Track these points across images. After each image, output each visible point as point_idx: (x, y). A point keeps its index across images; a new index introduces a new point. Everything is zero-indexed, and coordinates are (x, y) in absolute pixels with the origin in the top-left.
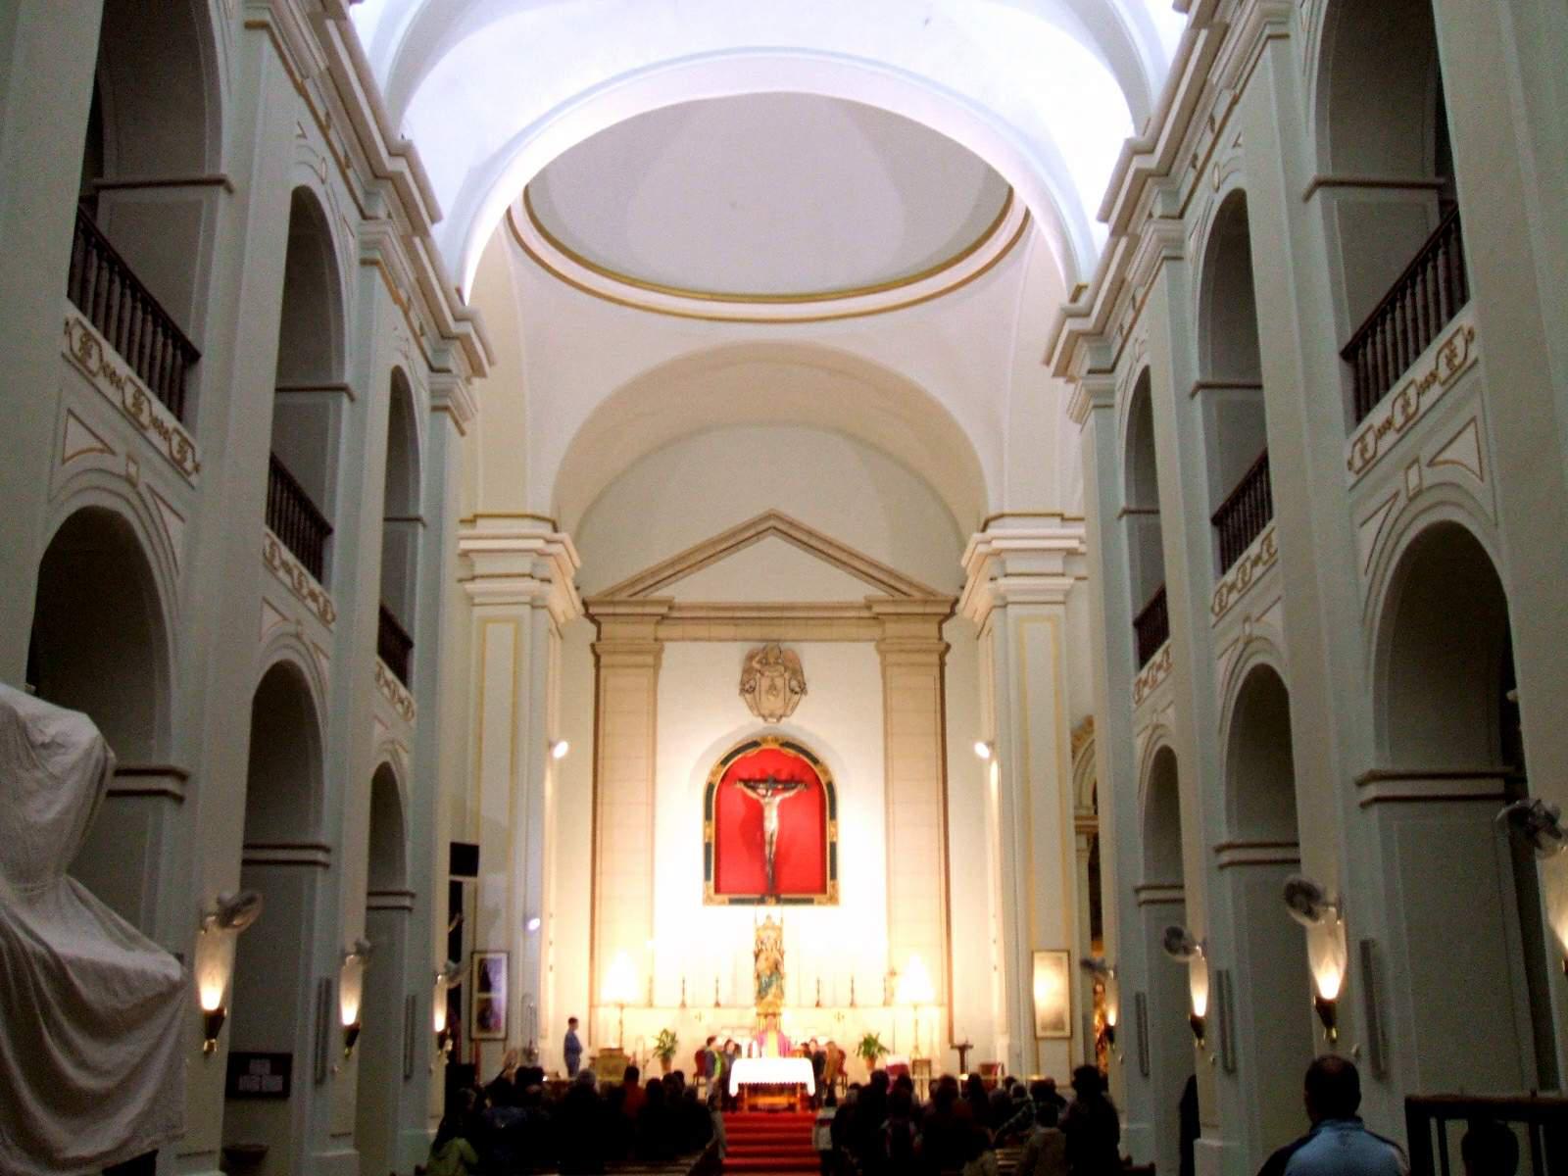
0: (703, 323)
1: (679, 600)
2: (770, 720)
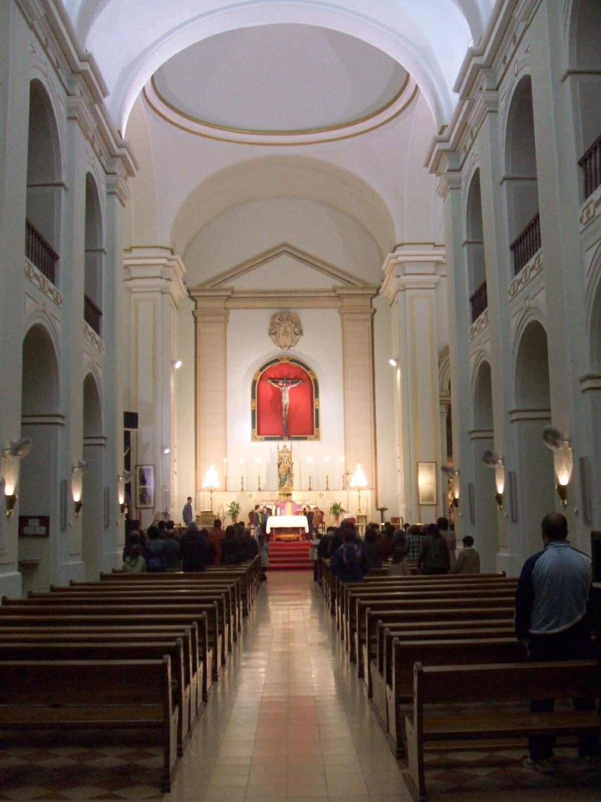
2: (284, 348)
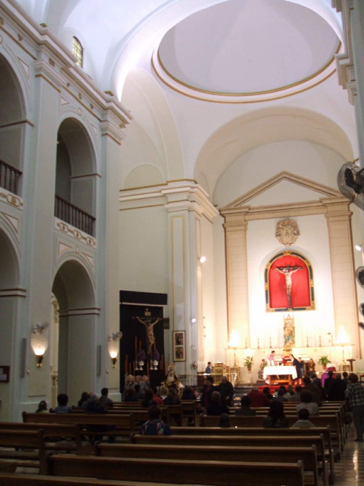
0: (242, 104)
1: (252, 206)
2: (287, 245)
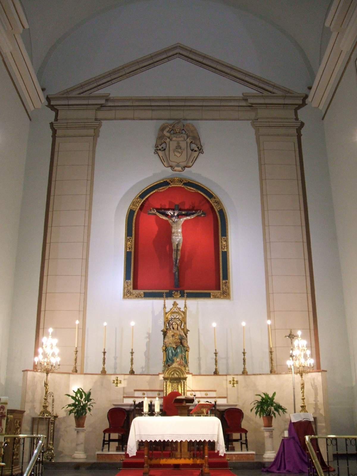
2: (176, 168)
